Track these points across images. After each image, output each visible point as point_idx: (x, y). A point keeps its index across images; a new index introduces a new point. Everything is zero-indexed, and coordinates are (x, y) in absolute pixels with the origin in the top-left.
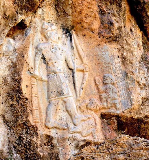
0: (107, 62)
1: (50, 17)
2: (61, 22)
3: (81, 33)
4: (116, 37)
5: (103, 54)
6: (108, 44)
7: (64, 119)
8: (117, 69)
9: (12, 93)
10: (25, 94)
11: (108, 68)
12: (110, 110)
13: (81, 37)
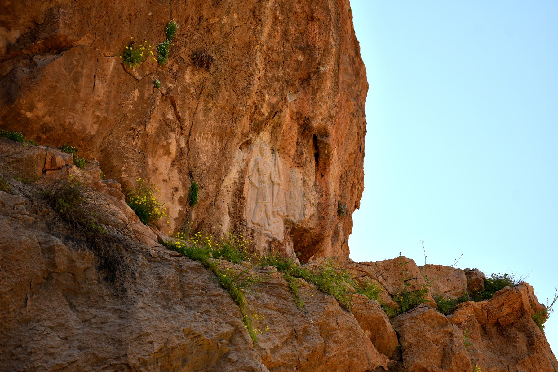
3: (282, 156)
9: (237, 192)
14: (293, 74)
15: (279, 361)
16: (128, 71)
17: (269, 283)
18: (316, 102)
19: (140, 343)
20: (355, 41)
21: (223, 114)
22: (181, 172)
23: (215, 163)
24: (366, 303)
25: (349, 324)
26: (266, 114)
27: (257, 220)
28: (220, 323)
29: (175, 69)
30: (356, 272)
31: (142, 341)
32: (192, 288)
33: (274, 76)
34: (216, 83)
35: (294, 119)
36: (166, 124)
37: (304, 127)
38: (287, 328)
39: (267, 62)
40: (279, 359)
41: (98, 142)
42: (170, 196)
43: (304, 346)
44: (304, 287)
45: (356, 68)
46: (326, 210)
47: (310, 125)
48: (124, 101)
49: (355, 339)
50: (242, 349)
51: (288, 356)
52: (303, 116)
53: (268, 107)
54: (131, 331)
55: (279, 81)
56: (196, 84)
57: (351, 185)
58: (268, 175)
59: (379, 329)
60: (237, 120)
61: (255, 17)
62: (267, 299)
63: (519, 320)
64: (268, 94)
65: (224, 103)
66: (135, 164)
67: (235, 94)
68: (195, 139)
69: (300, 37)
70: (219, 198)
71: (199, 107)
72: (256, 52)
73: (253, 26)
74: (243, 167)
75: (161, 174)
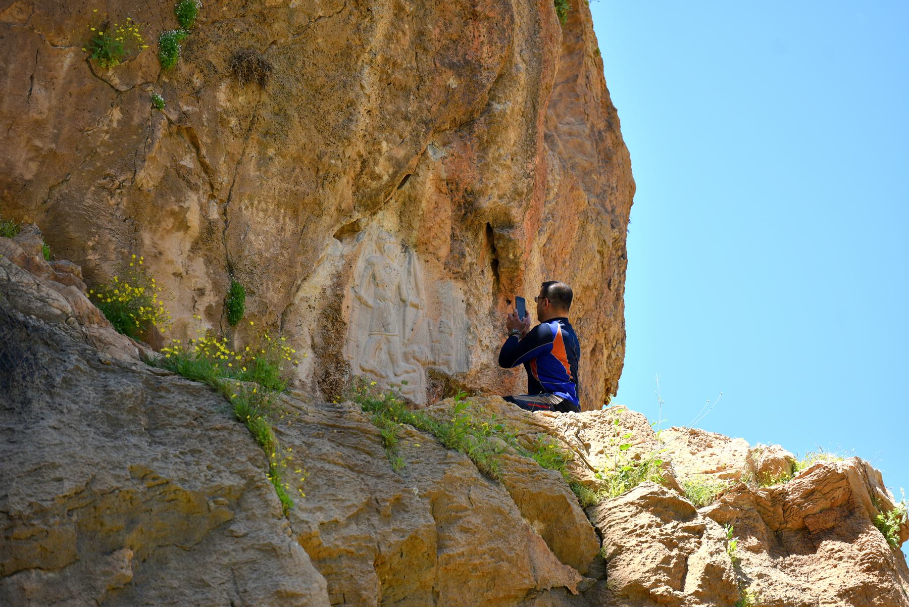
3: (424, 257)
4: (465, 274)
9: (329, 311)
14: (439, 110)
15: (338, 546)
16: (100, 75)
17: (338, 427)
18: (486, 164)
19: (37, 481)
20: (608, 106)
21: (298, 170)
22: (211, 263)
23: (281, 254)
24: (534, 471)
25: (495, 502)
26: (386, 178)
27: (372, 364)
28: (219, 472)
29: (197, 81)
30: (524, 426)
31: (43, 477)
32: (174, 416)
33: (398, 111)
34: (281, 113)
35: (444, 191)
36: (179, 175)
37: (466, 208)
38: (360, 495)
39: (384, 85)
40: (339, 543)
41: (41, 194)
42: (188, 302)
43: (392, 527)
44: (411, 439)
45: (605, 149)
47: (477, 204)
48: (90, 126)
49: (507, 529)
50: (259, 516)
51: (356, 539)
52: (462, 187)
53: (387, 163)
54: (22, 461)
55: (409, 120)
56: (241, 112)
57: (592, 345)
58: (394, 288)
59: (558, 519)
60: (326, 182)
61: (358, 4)
62: (327, 447)
63: (845, 521)
64: (387, 141)
65: (298, 151)
66: (114, 239)
67: (320, 136)
68: (240, 209)
69: (451, 46)
70: (291, 317)
71: (247, 152)
72: (362, 66)
73: (354, 19)
74: (341, 268)
75: (170, 262)
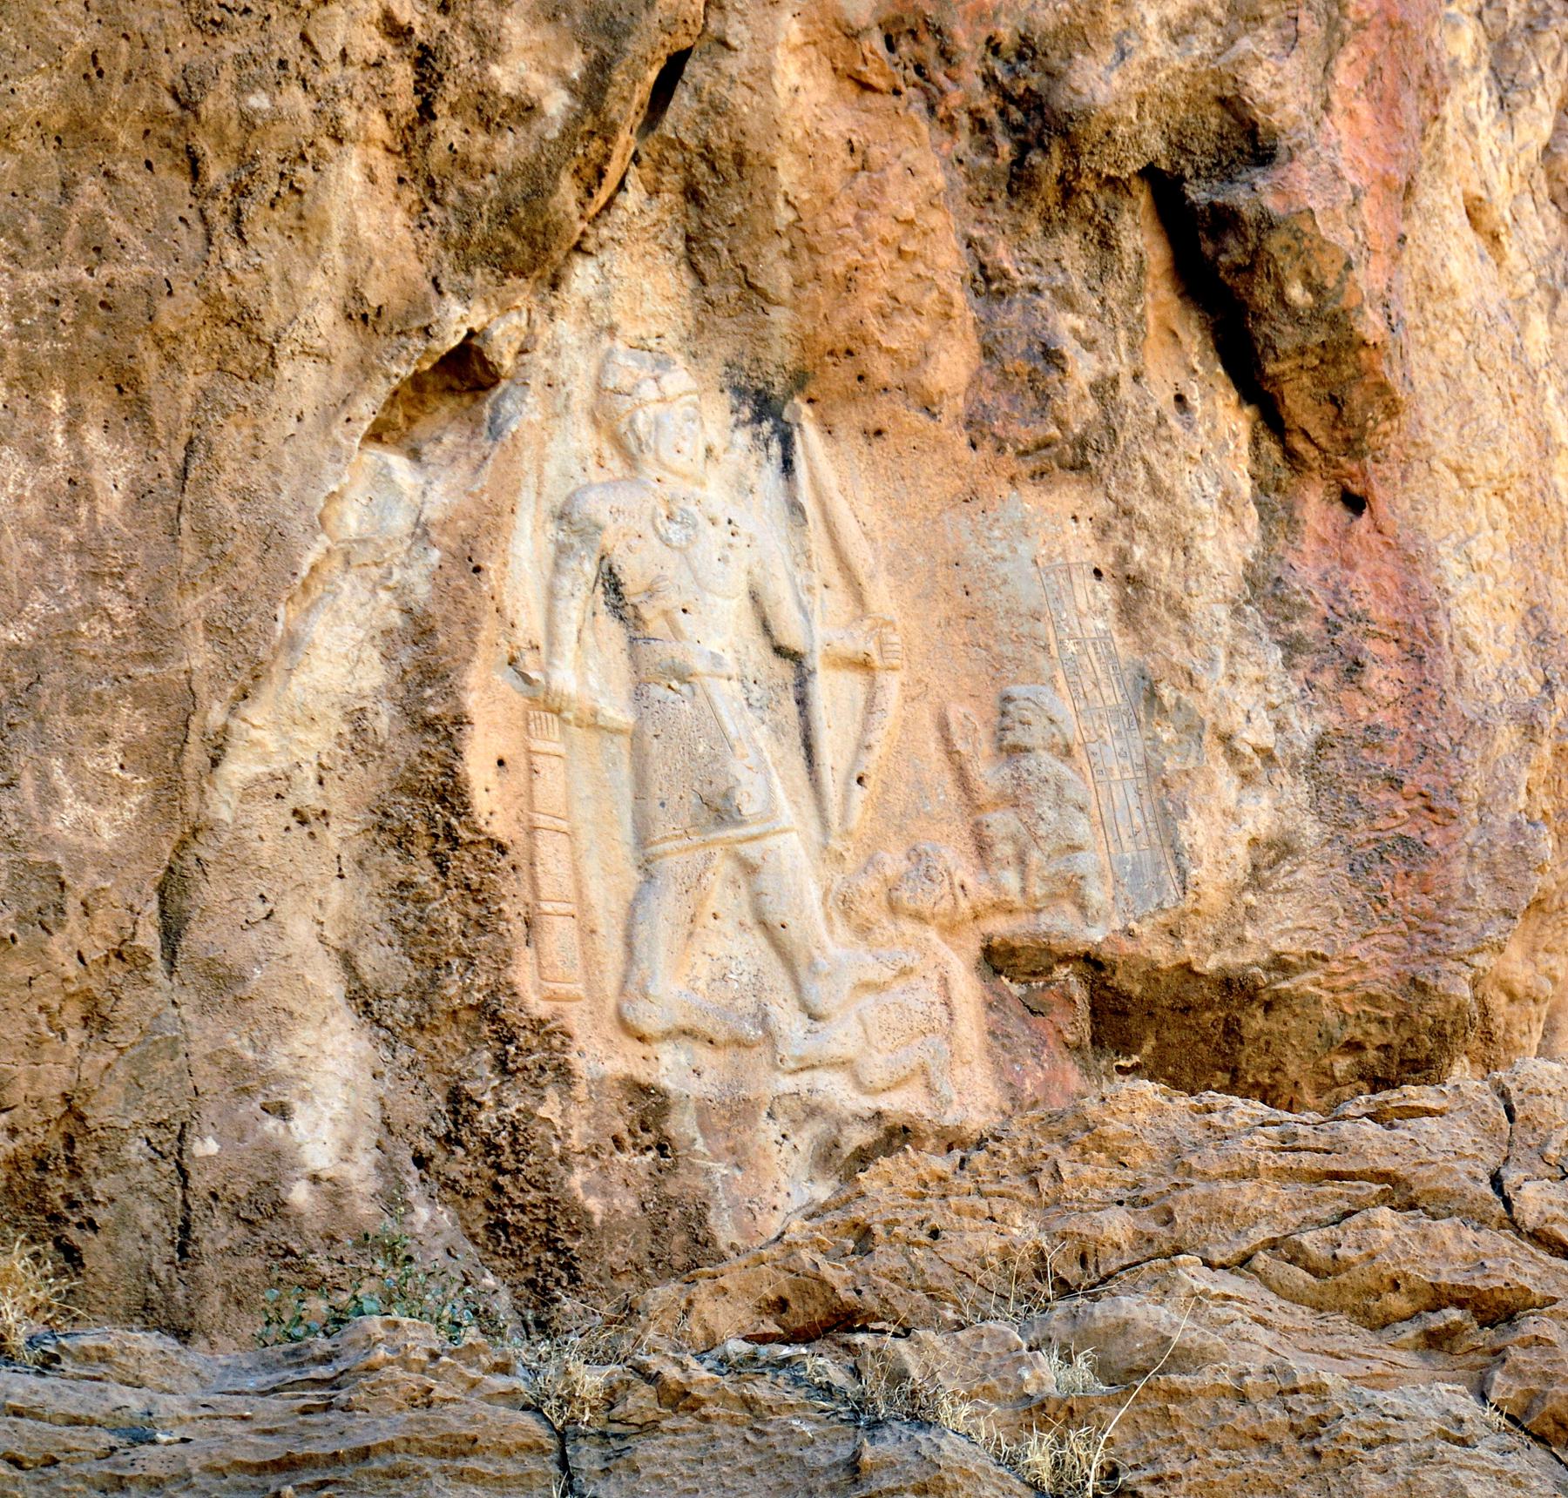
0: (1023, 610)
1: (653, 316)
2: (724, 350)
3: (857, 417)
5: (996, 551)
6: (1028, 490)
7: (745, 979)
8: (1091, 650)
9: (405, 809)
10: (486, 815)
11: (1029, 643)
12: (1045, 919)
13: (851, 442)
21: (90, 188)
23: (94, 609)
26: (556, 103)
46: (1418, 779)
47: (1061, 100)
70: (211, 891)
